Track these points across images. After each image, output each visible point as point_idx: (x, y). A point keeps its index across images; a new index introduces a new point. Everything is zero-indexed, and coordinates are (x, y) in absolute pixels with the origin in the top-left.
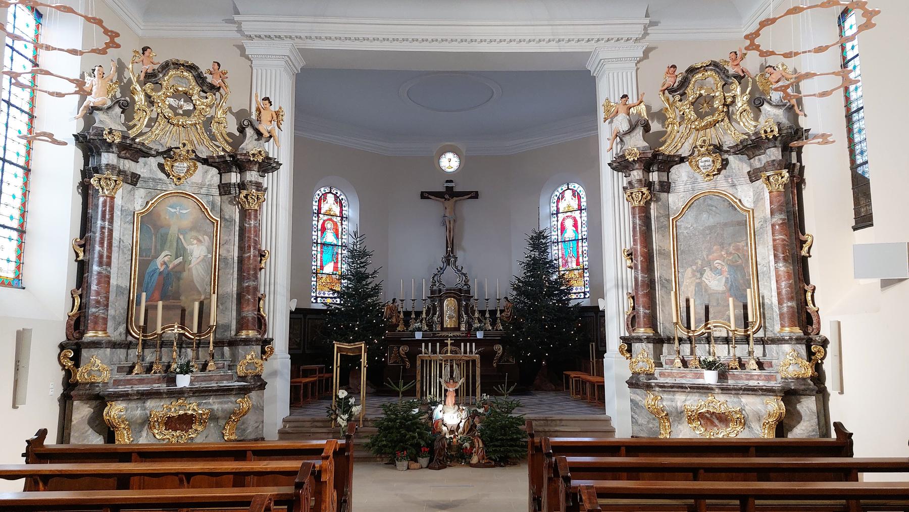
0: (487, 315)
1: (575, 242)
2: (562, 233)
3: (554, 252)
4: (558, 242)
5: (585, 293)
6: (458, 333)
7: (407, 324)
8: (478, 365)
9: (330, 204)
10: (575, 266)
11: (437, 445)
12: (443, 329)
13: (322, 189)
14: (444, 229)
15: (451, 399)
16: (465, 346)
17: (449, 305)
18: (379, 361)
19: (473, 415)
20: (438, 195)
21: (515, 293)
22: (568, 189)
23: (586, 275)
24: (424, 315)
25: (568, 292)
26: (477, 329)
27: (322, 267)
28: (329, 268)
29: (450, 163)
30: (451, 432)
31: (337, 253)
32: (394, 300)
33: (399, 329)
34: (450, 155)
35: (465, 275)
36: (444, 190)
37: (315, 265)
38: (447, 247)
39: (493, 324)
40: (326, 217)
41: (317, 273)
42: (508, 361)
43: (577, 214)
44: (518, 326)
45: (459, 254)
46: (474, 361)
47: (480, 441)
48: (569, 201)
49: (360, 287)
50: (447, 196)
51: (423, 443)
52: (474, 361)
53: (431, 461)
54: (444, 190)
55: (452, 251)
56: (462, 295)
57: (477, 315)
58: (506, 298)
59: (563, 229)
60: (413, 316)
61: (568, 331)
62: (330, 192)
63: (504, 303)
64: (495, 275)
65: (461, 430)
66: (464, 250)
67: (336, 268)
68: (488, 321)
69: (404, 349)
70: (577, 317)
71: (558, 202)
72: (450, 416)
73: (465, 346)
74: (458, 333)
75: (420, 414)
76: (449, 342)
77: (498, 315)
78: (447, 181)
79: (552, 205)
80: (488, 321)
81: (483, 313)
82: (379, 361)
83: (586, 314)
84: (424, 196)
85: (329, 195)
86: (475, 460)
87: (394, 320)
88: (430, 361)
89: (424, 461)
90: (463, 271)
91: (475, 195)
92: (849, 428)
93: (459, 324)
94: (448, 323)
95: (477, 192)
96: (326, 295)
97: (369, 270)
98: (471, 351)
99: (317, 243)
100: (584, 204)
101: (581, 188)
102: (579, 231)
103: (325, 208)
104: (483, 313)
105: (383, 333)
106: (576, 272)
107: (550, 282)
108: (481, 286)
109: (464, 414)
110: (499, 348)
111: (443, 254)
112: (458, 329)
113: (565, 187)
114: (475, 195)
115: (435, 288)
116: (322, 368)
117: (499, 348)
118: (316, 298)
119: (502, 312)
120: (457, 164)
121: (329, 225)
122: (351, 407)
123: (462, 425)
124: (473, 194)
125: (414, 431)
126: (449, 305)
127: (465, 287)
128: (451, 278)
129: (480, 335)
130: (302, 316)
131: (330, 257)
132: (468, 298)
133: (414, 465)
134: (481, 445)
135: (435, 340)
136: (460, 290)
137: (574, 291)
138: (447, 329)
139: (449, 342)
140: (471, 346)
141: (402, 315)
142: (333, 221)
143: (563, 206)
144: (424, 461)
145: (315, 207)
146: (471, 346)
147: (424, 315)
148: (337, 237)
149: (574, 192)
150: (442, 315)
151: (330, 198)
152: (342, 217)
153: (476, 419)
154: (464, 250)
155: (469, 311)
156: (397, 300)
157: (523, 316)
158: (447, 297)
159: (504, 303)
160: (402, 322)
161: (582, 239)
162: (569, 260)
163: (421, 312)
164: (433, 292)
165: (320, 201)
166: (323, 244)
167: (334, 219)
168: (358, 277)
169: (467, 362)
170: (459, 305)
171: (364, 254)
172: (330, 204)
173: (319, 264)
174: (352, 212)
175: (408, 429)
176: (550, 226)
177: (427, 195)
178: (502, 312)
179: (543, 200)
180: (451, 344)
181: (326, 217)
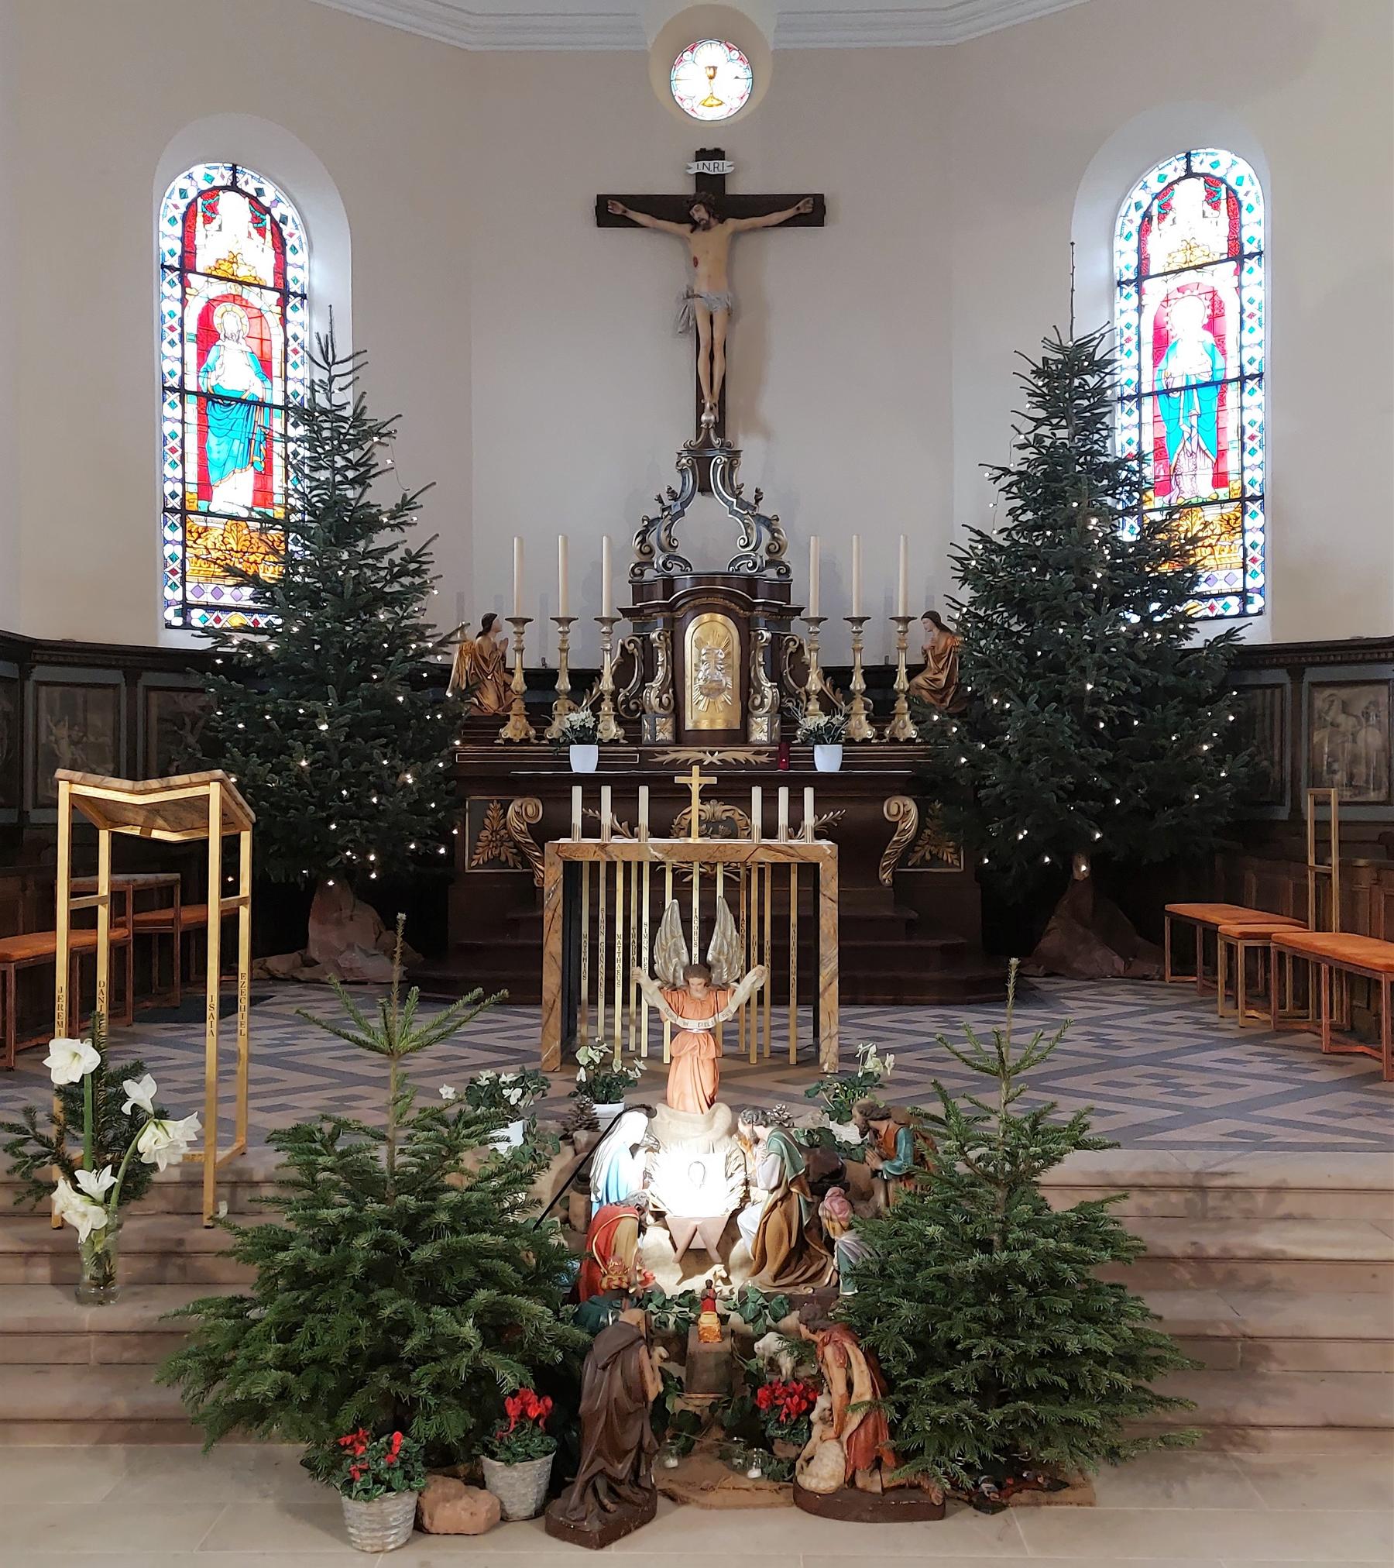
0: (858, 683)
1: (1212, 392)
2: (1158, 356)
3: (1127, 433)
4: (1139, 397)
5: (1244, 596)
6: (740, 754)
7: (539, 714)
8: (830, 886)
9: (229, 235)
10: (1205, 489)
11: (599, 1387)
12: (680, 736)
13: (199, 171)
14: (687, 345)
15: (691, 1075)
16: (770, 801)
17: (707, 642)
18: (426, 858)
19: (818, 1171)
20: (667, 209)
21: (966, 594)
22: (1189, 174)
23: (1255, 521)
24: (607, 684)
25: (1181, 588)
26: (820, 737)
27: (205, 489)
28: (234, 492)
29: (712, 84)
30: (694, 1258)
31: (268, 438)
32: (488, 621)
33: (506, 732)
34: (711, 53)
35: (769, 523)
36: (687, 189)
37: (175, 478)
38: (700, 410)
39: (881, 714)
40: (218, 289)
41: (184, 512)
42: (936, 860)
43: (1223, 278)
44: (981, 725)
45: (749, 445)
46: (810, 872)
47: (857, 1357)
48: (1194, 224)
49: (343, 560)
50: (700, 213)
51: (509, 1375)
52: (810, 872)
53: (556, 1487)
54: (687, 189)
55: (720, 427)
56: (757, 600)
57: (814, 683)
58: (933, 617)
59: (1162, 342)
60: (563, 684)
61: (1189, 744)
62: (233, 187)
63: (921, 634)
64: (891, 531)
65: (744, 1246)
66: (767, 434)
67: (262, 492)
68: (858, 705)
69: (523, 811)
70: (1222, 689)
71: (1144, 229)
72: (685, 1178)
73: (770, 801)
74: (740, 754)
75: (533, 1157)
76: (695, 782)
77: (901, 682)
78: (702, 155)
79: (1119, 244)
80: (858, 705)
81: (838, 677)
82: (426, 858)
83: (1251, 678)
84: (611, 212)
85: (227, 200)
86: (825, 1467)
87: (490, 700)
88: (611, 866)
89: (519, 1481)
90: (764, 509)
91: (810, 212)
93: (746, 714)
94: (704, 712)
95: (818, 201)
96: (227, 600)
97: (381, 495)
98: (795, 824)
99: (182, 391)
100: (1254, 231)
101: (1243, 168)
102: (1231, 345)
103: (210, 249)
104: (838, 677)
105: (440, 743)
106: (1212, 513)
107: (1119, 549)
108: (831, 576)
109: (766, 1168)
110: (904, 811)
111: (688, 434)
112: (740, 736)
113: (1174, 168)
114: (810, 212)
115: (650, 575)
116: (169, 888)
117: (904, 811)
118: (185, 608)
119: (913, 671)
120: (743, 87)
121: (227, 320)
122: (137, 1121)
123: (749, 1222)
124: (805, 207)
125: (455, 1302)
126: (707, 642)
127: (771, 573)
128: (712, 537)
129: (827, 759)
130: (115, 677)
131: (238, 447)
132: (784, 614)
133: (454, 1505)
134: (863, 1388)
135: (643, 779)
136: (751, 583)
137: (1202, 588)
138: (701, 738)
139: (695, 782)
140: (796, 801)
141: (518, 682)
142: (246, 306)
143: (1163, 247)
144: (519, 1481)
145: (169, 242)
146: (796, 801)
147: (607, 684)
148: (265, 366)
149: (1212, 182)
150: (676, 683)
151: (233, 207)
152: (284, 295)
153: (832, 1206)
154: (767, 434)
155: (785, 664)
156: (500, 620)
157: (1000, 684)
158: (699, 610)
159: (921, 634)
160: (518, 706)
161: (1242, 379)
162: (1185, 464)
163: (597, 674)
164: (640, 590)
165: (189, 217)
166: (207, 398)
167: (251, 295)
168: (339, 522)
169: (780, 871)
171: (361, 430)
172: (229, 235)
173: (192, 476)
174: (322, 271)
175: (430, 1289)
176: (1119, 325)
177: (618, 209)
178: (913, 671)
179: (1084, 226)
180: (707, 794)
181: (218, 289)
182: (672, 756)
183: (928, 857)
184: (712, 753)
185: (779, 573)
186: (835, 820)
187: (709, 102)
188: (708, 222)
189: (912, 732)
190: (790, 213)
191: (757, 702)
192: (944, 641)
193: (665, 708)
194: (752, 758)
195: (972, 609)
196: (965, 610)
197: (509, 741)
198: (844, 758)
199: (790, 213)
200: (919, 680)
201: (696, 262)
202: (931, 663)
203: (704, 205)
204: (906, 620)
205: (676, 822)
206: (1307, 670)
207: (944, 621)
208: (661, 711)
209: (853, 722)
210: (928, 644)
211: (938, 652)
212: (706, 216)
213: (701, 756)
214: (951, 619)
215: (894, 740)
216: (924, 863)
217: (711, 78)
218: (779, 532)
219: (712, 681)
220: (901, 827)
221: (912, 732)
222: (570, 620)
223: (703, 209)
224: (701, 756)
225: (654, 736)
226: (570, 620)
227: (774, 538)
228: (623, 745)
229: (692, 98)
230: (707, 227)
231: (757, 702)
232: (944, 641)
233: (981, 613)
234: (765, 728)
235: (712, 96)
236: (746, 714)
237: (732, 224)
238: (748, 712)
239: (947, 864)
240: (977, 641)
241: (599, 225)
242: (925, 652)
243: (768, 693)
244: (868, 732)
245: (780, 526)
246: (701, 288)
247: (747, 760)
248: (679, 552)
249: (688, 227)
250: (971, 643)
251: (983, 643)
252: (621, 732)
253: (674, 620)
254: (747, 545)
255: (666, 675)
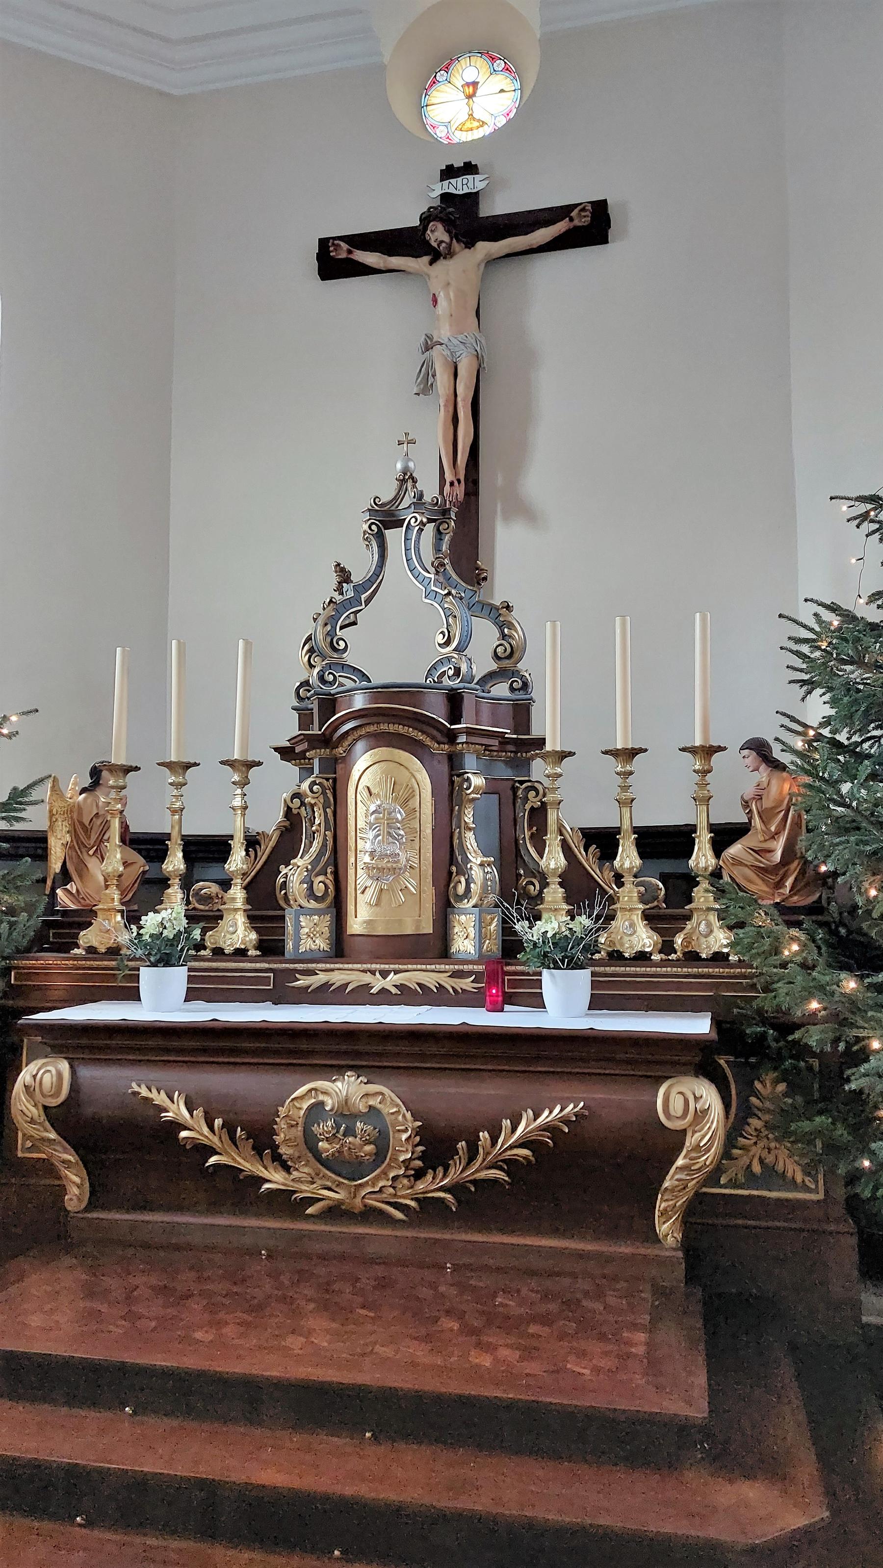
12: (340, 947)
29: (471, 106)
33: (88, 937)
34: (471, 69)
39: (666, 917)
77: (702, 858)
78: (449, 173)
84: (335, 262)
92: (348, 568)
93: (445, 908)
95: (600, 209)
124: (582, 220)
128: (407, 636)
132: (520, 744)
150: (335, 861)
170: (450, 796)
177: (342, 252)
178: (724, 836)
182: (322, 978)
183: (757, 1168)
184: (384, 974)
185: (512, 689)
186: (566, 1121)
187: (468, 125)
188: (450, 245)
189: (719, 939)
190: (561, 227)
191: (461, 889)
192: (781, 787)
193: (317, 899)
194: (448, 983)
195: (826, 732)
196: (812, 733)
197: (91, 950)
198: (594, 985)
199: (561, 227)
200: (735, 849)
201: (435, 301)
202: (757, 822)
203: (441, 220)
204: (709, 751)
205: (282, 1111)
206: (421, 778)
207: (777, 753)
208: (313, 904)
209: (620, 924)
210: (749, 791)
211: (767, 803)
212: (446, 238)
213: (367, 978)
214: (788, 748)
215: (692, 957)
216: (751, 1179)
217: (470, 97)
218: (511, 626)
219: (382, 857)
220: (690, 1141)
221: (719, 939)
222: (188, 766)
223: (440, 227)
224: (367, 978)
225: (297, 946)
226: (188, 766)
227: (504, 636)
228: (254, 959)
229: (447, 124)
230: (450, 254)
231: (461, 889)
232: (781, 787)
233: (842, 737)
234: (472, 932)
235: (471, 116)
236: (445, 908)
237: (484, 248)
238: (448, 904)
239: (793, 1185)
240: (835, 784)
241: (323, 279)
242: (746, 804)
243: (477, 873)
244: (644, 938)
245: (515, 616)
246: (444, 333)
247: (440, 987)
248: (350, 658)
249: (426, 259)
250: (823, 788)
251: (845, 788)
252: (253, 936)
253: (336, 760)
254: (448, 643)
255: (324, 845)
